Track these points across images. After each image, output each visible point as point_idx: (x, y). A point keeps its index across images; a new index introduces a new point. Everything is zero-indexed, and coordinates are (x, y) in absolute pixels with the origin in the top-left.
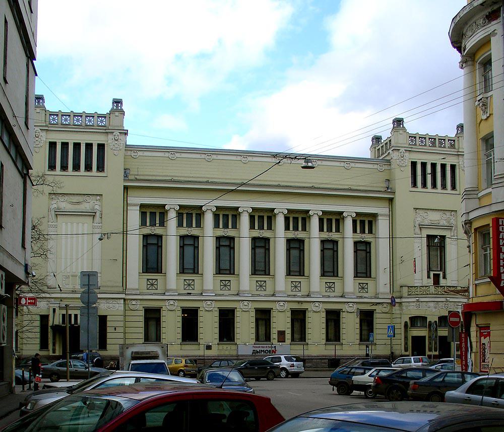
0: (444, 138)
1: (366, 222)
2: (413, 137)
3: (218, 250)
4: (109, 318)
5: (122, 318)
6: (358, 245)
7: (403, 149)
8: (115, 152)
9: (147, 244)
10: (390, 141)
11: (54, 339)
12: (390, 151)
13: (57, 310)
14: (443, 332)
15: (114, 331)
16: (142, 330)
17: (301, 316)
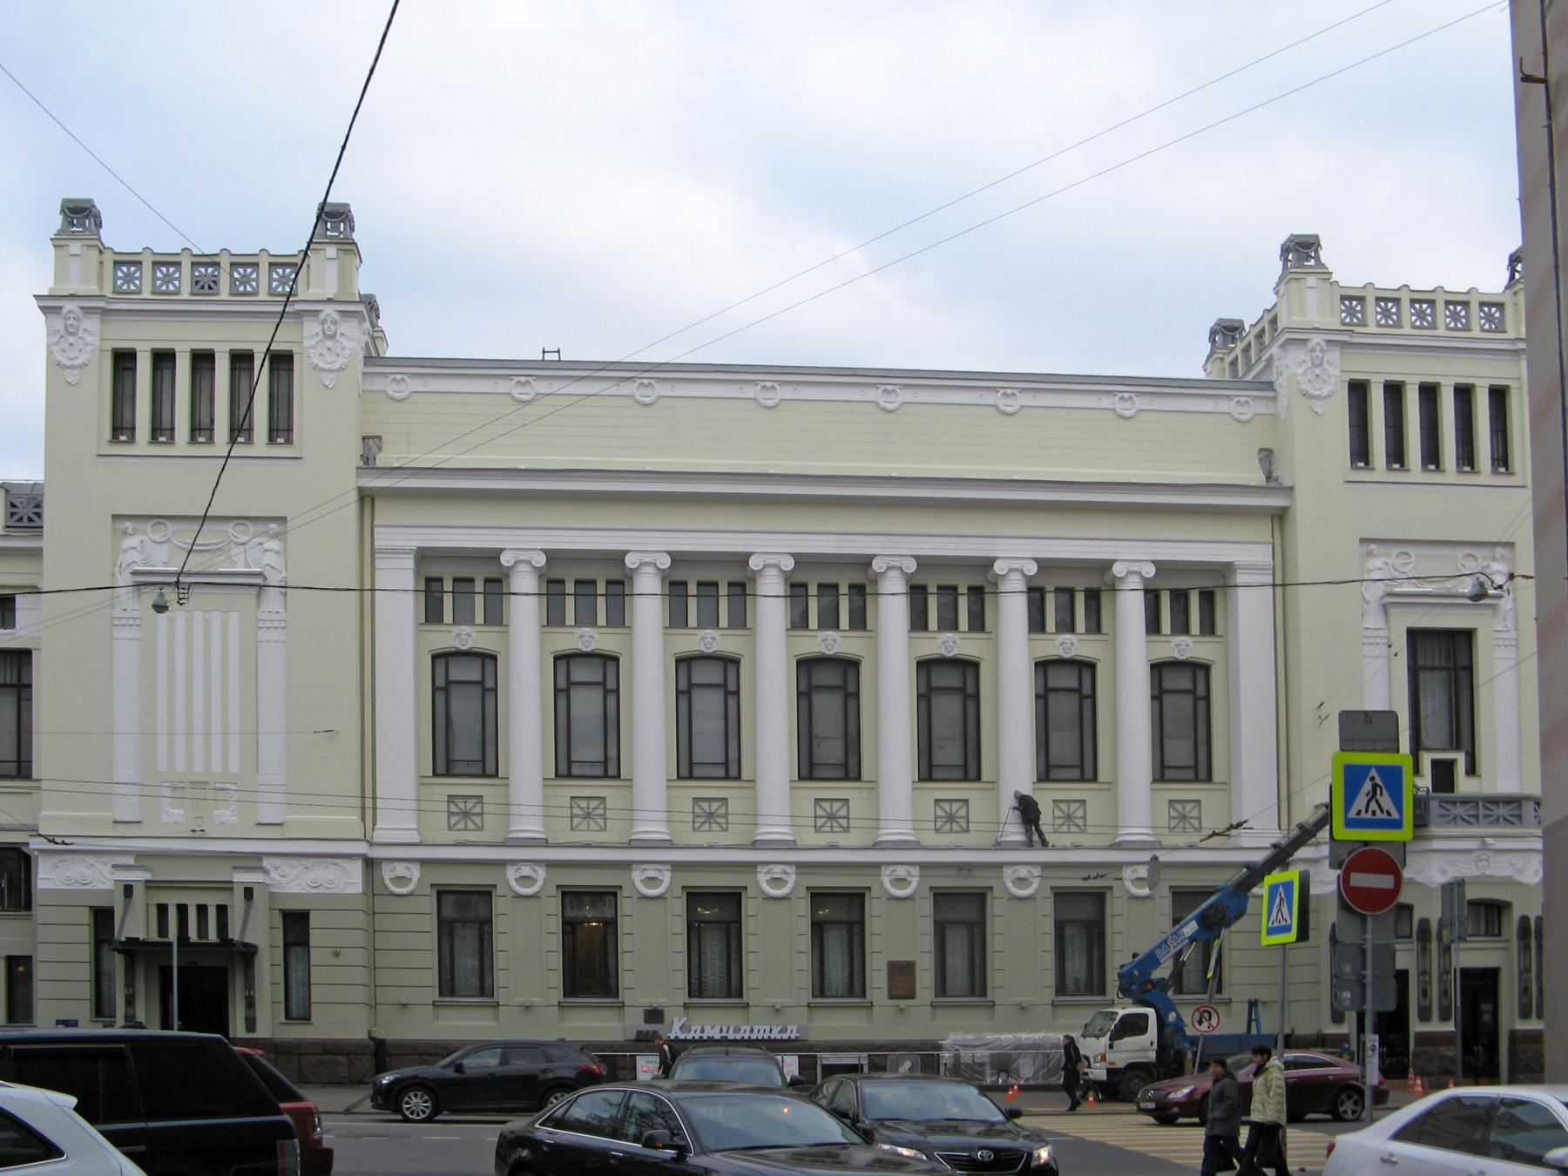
0: (1464, 298)
1: (1191, 597)
2: (1352, 300)
3: (804, 702)
4: (314, 920)
5: (360, 920)
6: (1166, 674)
7: (1318, 339)
8: (328, 379)
9: (449, 683)
10: (1274, 321)
11: (130, 982)
12: (1274, 350)
13: (138, 891)
14: (1474, 955)
15: (333, 961)
16: (431, 959)
17: (967, 912)
